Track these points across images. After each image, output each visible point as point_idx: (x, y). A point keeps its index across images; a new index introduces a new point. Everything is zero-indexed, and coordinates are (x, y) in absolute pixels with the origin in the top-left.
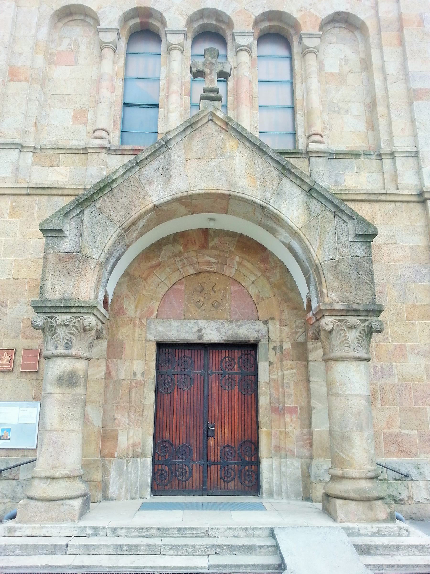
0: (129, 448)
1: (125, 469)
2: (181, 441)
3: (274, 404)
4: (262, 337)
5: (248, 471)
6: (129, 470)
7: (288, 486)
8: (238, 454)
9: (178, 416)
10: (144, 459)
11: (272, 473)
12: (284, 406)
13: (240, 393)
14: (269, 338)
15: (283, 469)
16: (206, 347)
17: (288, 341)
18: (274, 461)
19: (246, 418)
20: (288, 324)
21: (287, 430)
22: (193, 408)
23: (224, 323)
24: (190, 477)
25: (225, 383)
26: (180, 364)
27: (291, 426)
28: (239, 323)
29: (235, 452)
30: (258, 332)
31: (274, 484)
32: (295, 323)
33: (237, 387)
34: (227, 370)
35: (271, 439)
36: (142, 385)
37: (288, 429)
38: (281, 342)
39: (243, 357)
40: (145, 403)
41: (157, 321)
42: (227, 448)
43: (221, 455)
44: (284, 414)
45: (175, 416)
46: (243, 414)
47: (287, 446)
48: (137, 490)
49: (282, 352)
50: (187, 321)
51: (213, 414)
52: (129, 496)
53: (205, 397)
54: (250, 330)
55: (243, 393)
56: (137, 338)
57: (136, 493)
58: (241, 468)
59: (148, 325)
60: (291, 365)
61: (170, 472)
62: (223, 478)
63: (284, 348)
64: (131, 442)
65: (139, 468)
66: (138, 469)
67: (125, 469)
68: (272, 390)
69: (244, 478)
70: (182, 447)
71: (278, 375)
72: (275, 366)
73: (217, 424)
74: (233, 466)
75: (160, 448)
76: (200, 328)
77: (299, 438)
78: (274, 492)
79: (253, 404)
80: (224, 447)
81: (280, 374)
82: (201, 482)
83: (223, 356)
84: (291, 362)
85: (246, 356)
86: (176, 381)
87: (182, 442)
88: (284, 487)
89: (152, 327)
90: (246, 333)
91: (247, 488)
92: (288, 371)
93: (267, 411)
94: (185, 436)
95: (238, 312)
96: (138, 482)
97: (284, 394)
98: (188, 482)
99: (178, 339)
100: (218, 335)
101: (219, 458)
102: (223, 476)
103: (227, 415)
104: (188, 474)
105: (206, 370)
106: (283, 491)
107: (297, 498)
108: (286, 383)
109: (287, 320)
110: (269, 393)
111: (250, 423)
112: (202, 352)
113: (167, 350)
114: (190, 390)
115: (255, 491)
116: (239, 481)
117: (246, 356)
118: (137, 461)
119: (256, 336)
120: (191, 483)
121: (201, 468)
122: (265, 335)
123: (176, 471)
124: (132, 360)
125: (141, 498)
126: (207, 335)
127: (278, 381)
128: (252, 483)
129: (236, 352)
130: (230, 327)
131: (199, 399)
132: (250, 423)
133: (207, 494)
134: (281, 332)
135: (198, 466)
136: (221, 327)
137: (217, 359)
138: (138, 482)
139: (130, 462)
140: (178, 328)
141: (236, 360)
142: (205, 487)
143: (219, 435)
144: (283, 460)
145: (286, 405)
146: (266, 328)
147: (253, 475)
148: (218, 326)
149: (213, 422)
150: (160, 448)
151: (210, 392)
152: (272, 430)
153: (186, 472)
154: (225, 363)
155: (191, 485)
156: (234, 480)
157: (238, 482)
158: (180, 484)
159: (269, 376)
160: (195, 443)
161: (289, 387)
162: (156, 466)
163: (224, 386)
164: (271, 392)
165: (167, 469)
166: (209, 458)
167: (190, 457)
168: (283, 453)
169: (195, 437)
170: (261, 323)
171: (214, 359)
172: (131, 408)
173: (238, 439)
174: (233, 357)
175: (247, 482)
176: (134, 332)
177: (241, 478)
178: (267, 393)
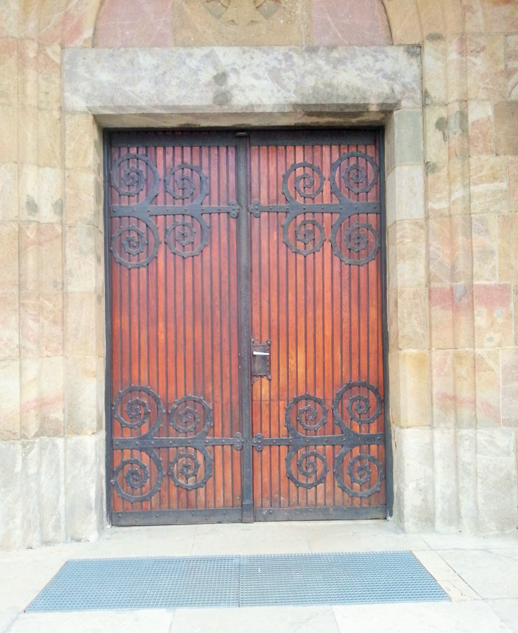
0: (28, 411)
1: (18, 468)
2: (181, 390)
3: (441, 281)
4: (403, 93)
5: (360, 458)
6: (32, 471)
7: (480, 500)
8: (333, 416)
9: (171, 325)
10: (75, 439)
11: (432, 466)
12: (472, 286)
13: (336, 260)
14: (425, 94)
15: (466, 456)
16: (240, 137)
17: (484, 97)
18: (437, 434)
19: (355, 326)
20: (483, 49)
21: (478, 351)
22: (209, 304)
23: (291, 56)
24: (207, 477)
25: (296, 236)
26: (170, 188)
27: (491, 339)
28: (335, 54)
29: (325, 412)
30: (393, 79)
31: (438, 494)
32: (506, 45)
33: (327, 246)
34: (300, 200)
35: (431, 376)
36: (57, 237)
37: (482, 347)
38: (464, 101)
39: (344, 163)
40: (70, 288)
41: (92, 53)
42: (304, 402)
43: (288, 421)
44: (471, 307)
45: (161, 325)
46: (346, 315)
47: (478, 393)
48: (58, 521)
49: (464, 130)
50: (182, 50)
51: (265, 316)
52: (35, 538)
53: (243, 274)
54: (368, 75)
55: (346, 260)
56: (32, 102)
57: (56, 528)
58: (342, 450)
59: (67, 67)
60: (492, 168)
61: (153, 465)
62: (295, 477)
63: (472, 117)
64: (32, 394)
65: (62, 463)
66: (58, 465)
67: (18, 468)
68: (434, 244)
69: (351, 475)
70: (183, 404)
71: (453, 199)
72: (443, 173)
73: (275, 343)
74: (320, 448)
75: (125, 409)
76: (220, 72)
77: (514, 371)
78: (438, 514)
79: (373, 289)
80: (296, 401)
81: (458, 193)
82: (238, 488)
83: (291, 162)
84: (493, 160)
85: (353, 162)
86: (161, 232)
87: (183, 390)
88: (466, 503)
89: (81, 70)
90: (357, 82)
91: (357, 500)
92: (485, 185)
93: (417, 301)
94: (190, 375)
95: (333, 25)
96: (62, 500)
97: (470, 252)
98: (202, 491)
99: (155, 107)
100: (275, 90)
101: (284, 429)
102: (294, 473)
103: (301, 320)
104: (201, 471)
105: (243, 199)
106: (463, 512)
107: (502, 530)
108: (477, 220)
109: (481, 34)
110: (423, 252)
111: (363, 338)
112: (230, 154)
113: (133, 151)
114: (200, 257)
115: (377, 507)
116: (336, 484)
117: (353, 162)
118: (55, 445)
119: (387, 90)
120: (210, 491)
121: (237, 454)
122: (413, 89)
123: (170, 464)
124: (22, 164)
125: (73, 539)
126: (243, 90)
127: (450, 216)
128: (370, 487)
129: (326, 150)
130: (310, 66)
131: (225, 278)
132: (363, 338)
133: (255, 517)
134: (463, 71)
135: (228, 449)
136: (283, 66)
137: (272, 170)
138: (62, 500)
139: (32, 448)
140: (156, 74)
141: (326, 173)
142: (247, 502)
143: (283, 370)
144: (464, 432)
145: (476, 282)
146: (416, 67)
147: (374, 470)
148: (274, 63)
149: (265, 338)
150: (125, 409)
151: (255, 261)
152: (434, 354)
153: (197, 466)
154: (296, 180)
155: (211, 498)
156: (325, 483)
157: (334, 486)
158: (183, 495)
159: (425, 205)
160: (218, 392)
161: (487, 231)
162: (117, 454)
163: (292, 243)
164: (432, 249)
165: (145, 460)
166: (256, 428)
167: (206, 429)
168: (465, 413)
169: (218, 378)
170: (400, 54)
171: (264, 170)
172: (26, 301)
173: (333, 381)
174: (317, 164)
175: (356, 485)
176: (24, 82)
177: (342, 478)
178: (417, 252)
